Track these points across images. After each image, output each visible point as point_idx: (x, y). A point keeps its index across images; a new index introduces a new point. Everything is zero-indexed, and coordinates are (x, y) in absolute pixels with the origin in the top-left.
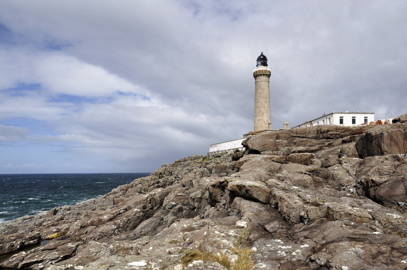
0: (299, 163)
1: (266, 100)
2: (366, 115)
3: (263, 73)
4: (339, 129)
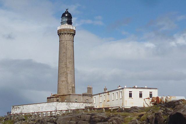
0: (132, 108)
1: (70, 60)
2: (151, 90)
3: (68, 32)
4: (100, 117)
